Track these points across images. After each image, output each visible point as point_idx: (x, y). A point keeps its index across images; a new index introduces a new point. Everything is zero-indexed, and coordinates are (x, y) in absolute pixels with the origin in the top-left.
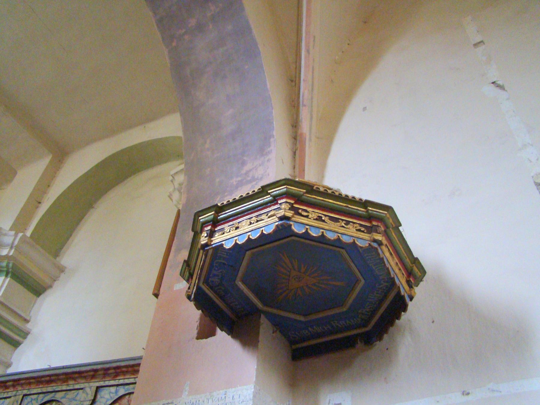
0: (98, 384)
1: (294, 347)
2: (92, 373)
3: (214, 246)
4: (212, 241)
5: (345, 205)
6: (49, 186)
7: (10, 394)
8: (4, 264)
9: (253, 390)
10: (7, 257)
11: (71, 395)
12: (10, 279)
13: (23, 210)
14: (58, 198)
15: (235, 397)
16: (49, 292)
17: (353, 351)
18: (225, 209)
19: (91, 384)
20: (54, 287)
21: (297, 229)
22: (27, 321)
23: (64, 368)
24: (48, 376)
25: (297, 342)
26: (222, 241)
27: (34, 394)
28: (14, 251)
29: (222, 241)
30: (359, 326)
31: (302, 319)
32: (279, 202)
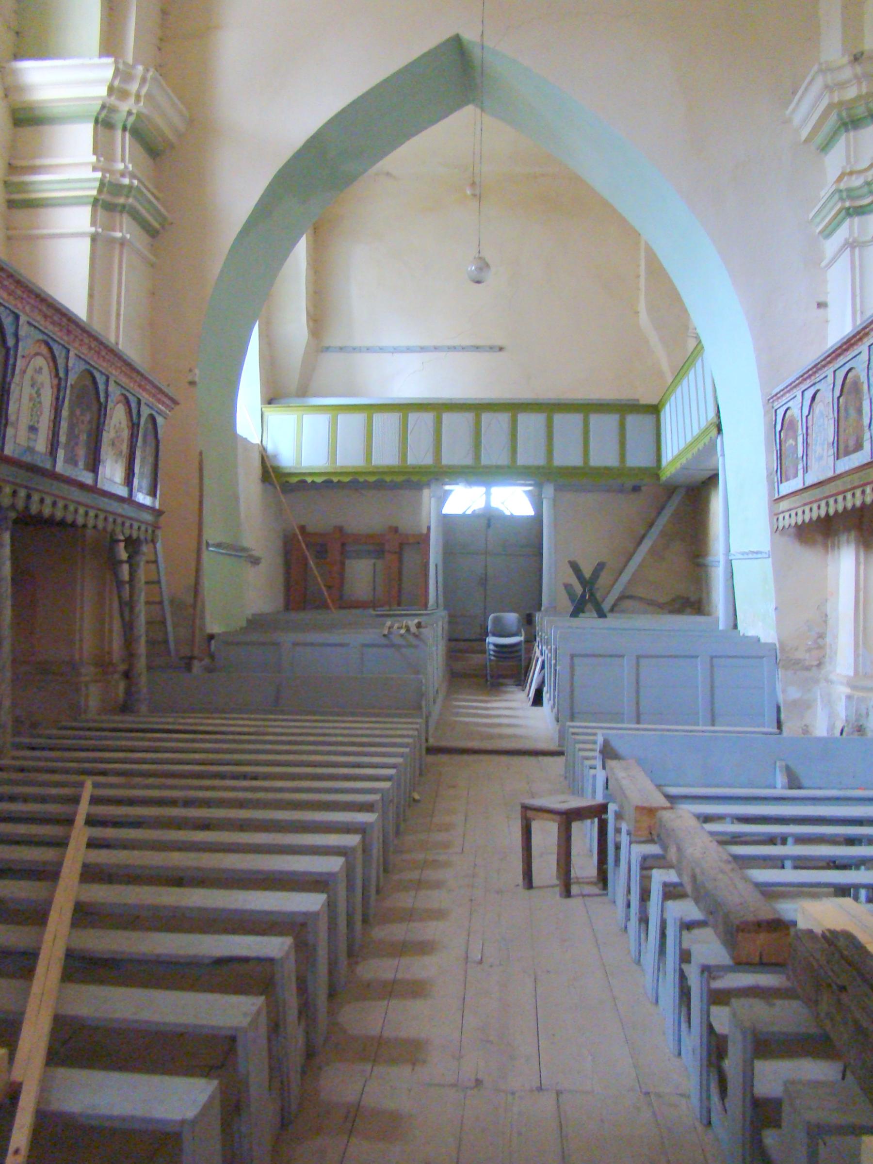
10: (859, 97)
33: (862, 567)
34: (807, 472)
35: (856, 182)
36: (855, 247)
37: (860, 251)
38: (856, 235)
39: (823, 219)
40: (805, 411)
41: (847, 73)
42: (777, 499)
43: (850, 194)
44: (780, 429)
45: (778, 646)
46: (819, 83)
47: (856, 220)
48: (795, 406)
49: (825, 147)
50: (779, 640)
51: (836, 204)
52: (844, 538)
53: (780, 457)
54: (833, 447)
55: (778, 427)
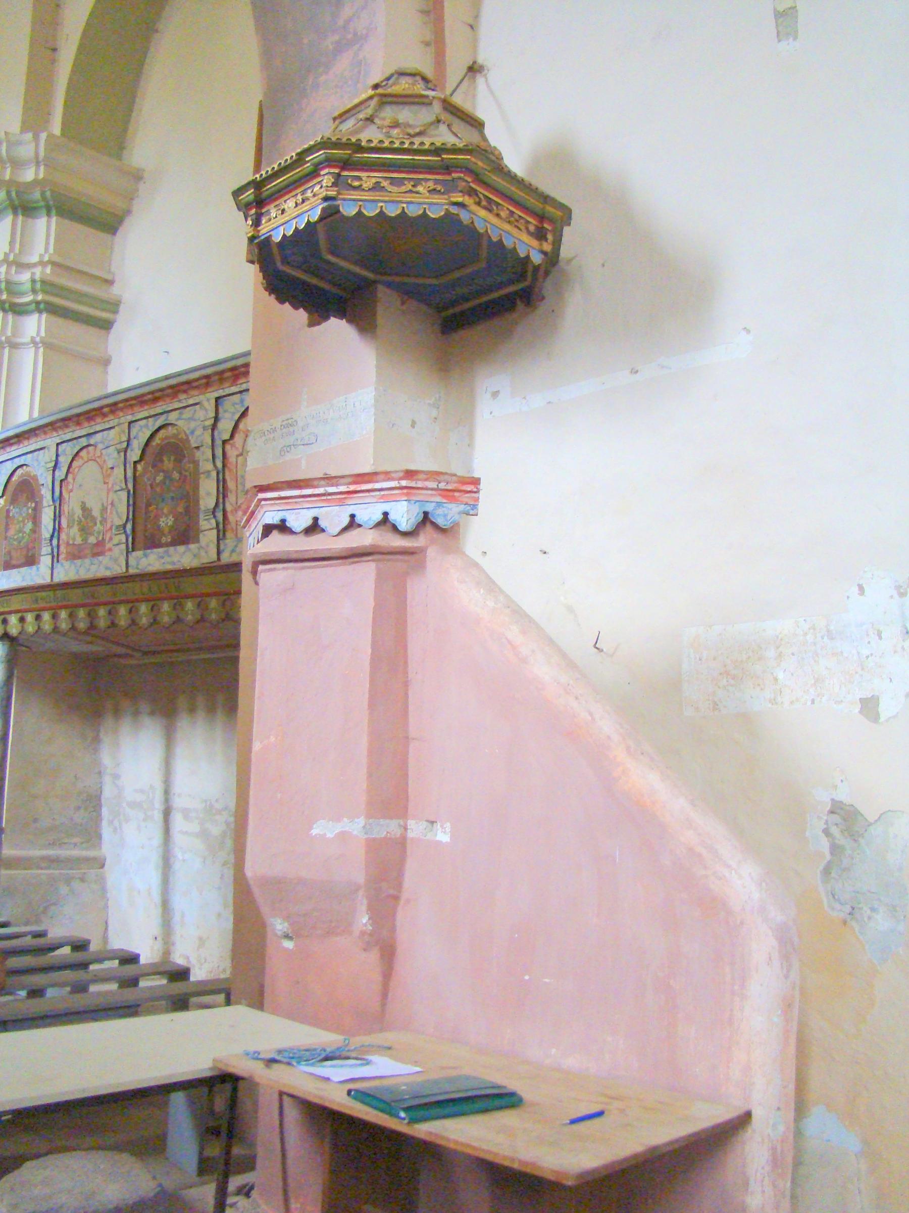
0: (216, 395)
1: (444, 314)
2: (204, 381)
3: (262, 238)
4: (259, 231)
5: (411, 157)
6: (55, 50)
7: (111, 424)
8: (37, 195)
9: (374, 393)
10: (36, 182)
11: (187, 413)
12: (57, 219)
14: (85, 35)
15: (356, 404)
16: (128, 222)
17: (515, 315)
18: (266, 183)
19: (208, 395)
20: (135, 209)
21: (349, 210)
22: (110, 283)
23: (167, 378)
24: (149, 393)
25: (446, 308)
26: (270, 231)
27: (141, 419)
29: (270, 231)
30: (511, 282)
31: (434, 281)
32: (322, 173)
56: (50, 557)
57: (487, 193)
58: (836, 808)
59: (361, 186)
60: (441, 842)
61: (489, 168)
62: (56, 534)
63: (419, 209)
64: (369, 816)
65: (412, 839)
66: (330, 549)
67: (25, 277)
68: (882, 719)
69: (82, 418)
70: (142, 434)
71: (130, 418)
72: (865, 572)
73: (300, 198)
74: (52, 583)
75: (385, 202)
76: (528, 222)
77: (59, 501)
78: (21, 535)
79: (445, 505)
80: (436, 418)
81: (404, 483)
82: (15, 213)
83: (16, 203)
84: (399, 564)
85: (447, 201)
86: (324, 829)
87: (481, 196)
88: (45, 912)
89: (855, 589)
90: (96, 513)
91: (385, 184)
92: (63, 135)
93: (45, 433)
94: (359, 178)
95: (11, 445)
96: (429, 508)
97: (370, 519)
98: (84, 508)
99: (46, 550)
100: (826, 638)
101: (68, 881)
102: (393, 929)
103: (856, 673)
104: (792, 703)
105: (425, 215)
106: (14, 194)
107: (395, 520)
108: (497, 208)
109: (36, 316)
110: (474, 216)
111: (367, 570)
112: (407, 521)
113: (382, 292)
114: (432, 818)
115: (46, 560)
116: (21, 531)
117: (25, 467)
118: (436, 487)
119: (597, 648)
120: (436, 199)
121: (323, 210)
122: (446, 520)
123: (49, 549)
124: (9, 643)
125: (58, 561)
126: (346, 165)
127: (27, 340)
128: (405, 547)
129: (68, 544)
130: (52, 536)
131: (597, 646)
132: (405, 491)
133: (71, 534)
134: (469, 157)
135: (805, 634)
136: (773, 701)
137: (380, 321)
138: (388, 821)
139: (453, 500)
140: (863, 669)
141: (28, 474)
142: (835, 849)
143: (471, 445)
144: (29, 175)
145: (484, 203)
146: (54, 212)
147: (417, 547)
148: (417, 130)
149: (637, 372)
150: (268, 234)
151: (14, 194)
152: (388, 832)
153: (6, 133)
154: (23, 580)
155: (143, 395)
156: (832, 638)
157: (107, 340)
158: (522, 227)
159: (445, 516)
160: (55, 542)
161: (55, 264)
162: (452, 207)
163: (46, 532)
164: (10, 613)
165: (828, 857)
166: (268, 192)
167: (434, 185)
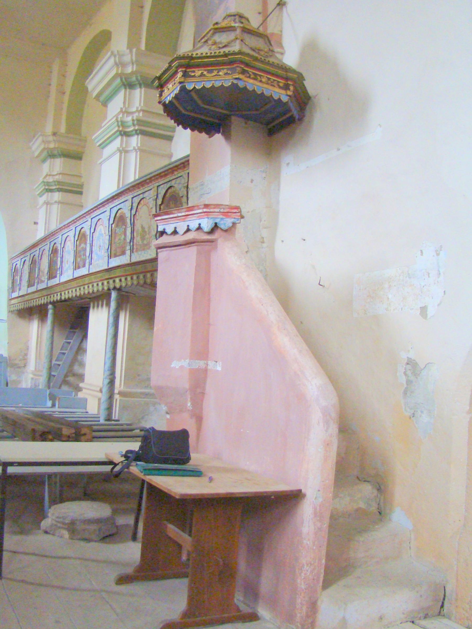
3: (163, 102)
5: (215, 59)
8: (134, 79)
9: (230, 168)
10: (132, 73)
11: (178, 180)
13: (131, 19)
21: (190, 87)
28: (136, 66)
33: (40, 328)
34: (91, 265)
35: (51, 179)
36: (48, 204)
37: (124, 154)
38: (49, 200)
39: (39, 190)
40: (92, 231)
41: (51, 138)
42: (11, 299)
43: (48, 184)
44: (77, 239)
45: (8, 358)
46: (41, 139)
47: (50, 194)
48: (18, 263)
49: (44, 161)
50: (9, 357)
51: (42, 187)
52: (35, 316)
53: (13, 283)
54: (47, 275)
55: (13, 271)
56: (129, 251)
57: (254, 71)
58: (410, 362)
59: (195, 75)
60: (218, 370)
61: (252, 60)
62: (132, 240)
63: (220, 83)
64: (191, 359)
65: (209, 369)
66: (179, 241)
67: (130, 119)
68: (429, 317)
69: (140, 185)
70: (162, 191)
71: (157, 184)
72: (423, 244)
73: (173, 83)
74: (131, 263)
75: (215, 81)
76: (278, 82)
77: (133, 225)
78: (120, 241)
79: (224, 219)
80: (265, 177)
81: (205, 210)
82: (126, 89)
83: (126, 83)
84: (207, 247)
85: (232, 78)
86: (176, 364)
87: (251, 73)
88: (143, 418)
89: (419, 253)
90: (146, 230)
91: (205, 73)
92: (146, 49)
93: (127, 193)
94: (194, 72)
95: (115, 199)
96: (217, 221)
97: (194, 227)
98: (143, 228)
99: (128, 248)
100: (407, 277)
101: (154, 404)
102: (201, 409)
103: (419, 294)
104: (394, 310)
105: (222, 85)
106: (124, 79)
107: (203, 227)
108: (260, 77)
109: (136, 137)
110: (246, 84)
111: (193, 250)
112: (207, 227)
113: (233, 118)
114: (216, 361)
115: (128, 252)
116: (120, 239)
117: (121, 209)
118: (219, 211)
119: (321, 285)
120: (227, 77)
121: (180, 88)
122: (225, 226)
123: (129, 247)
124: (117, 291)
125: (133, 252)
126: (188, 66)
127: (132, 148)
128: (208, 239)
129: (136, 244)
130: (130, 241)
131: (320, 284)
132: (206, 214)
133: (138, 239)
134: (240, 56)
135: (400, 276)
136: (387, 309)
137: (233, 133)
138: (199, 361)
139: (228, 216)
140: (422, 292)
141: (122, 213)
142: (409, 382)
143: (279, 190)
144: (129, 70)
145: (252, 76)
146: (143, 86)
147: (213, 239)
148: (224, 45)
149: (339, 150)
150: (164, 101)
151: (124, 79)
152: (199, 366)
153: (118, 51)
154: (121, 262)
155: (160, 173)
156: (410, 278)
157: (171, 144)
158: (275, 85)
159: (225, 224)
160: (132, 244)
161: (143, 111)
162: (235, 80)
163: (128, 240)
164: (116, 277)
165: (405, 386)
166: (165, 80)
167: (227, 71)
